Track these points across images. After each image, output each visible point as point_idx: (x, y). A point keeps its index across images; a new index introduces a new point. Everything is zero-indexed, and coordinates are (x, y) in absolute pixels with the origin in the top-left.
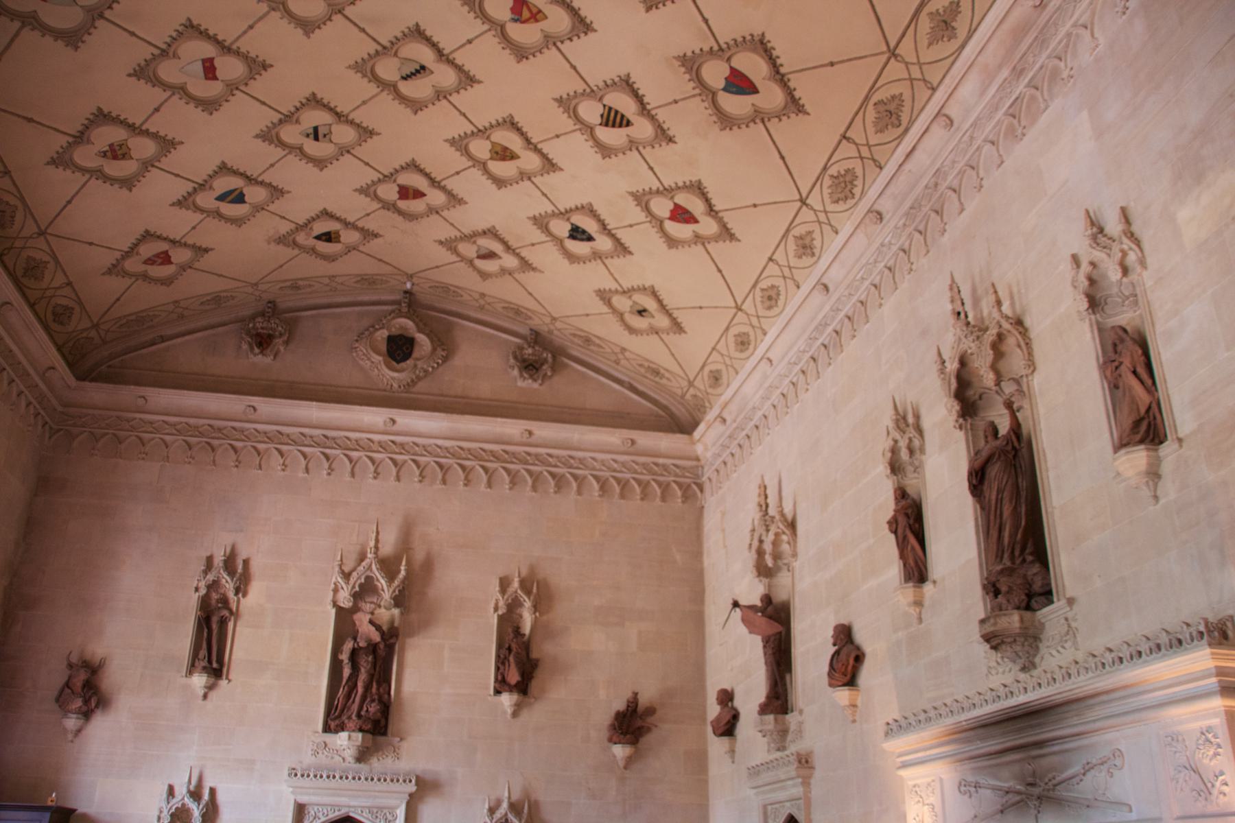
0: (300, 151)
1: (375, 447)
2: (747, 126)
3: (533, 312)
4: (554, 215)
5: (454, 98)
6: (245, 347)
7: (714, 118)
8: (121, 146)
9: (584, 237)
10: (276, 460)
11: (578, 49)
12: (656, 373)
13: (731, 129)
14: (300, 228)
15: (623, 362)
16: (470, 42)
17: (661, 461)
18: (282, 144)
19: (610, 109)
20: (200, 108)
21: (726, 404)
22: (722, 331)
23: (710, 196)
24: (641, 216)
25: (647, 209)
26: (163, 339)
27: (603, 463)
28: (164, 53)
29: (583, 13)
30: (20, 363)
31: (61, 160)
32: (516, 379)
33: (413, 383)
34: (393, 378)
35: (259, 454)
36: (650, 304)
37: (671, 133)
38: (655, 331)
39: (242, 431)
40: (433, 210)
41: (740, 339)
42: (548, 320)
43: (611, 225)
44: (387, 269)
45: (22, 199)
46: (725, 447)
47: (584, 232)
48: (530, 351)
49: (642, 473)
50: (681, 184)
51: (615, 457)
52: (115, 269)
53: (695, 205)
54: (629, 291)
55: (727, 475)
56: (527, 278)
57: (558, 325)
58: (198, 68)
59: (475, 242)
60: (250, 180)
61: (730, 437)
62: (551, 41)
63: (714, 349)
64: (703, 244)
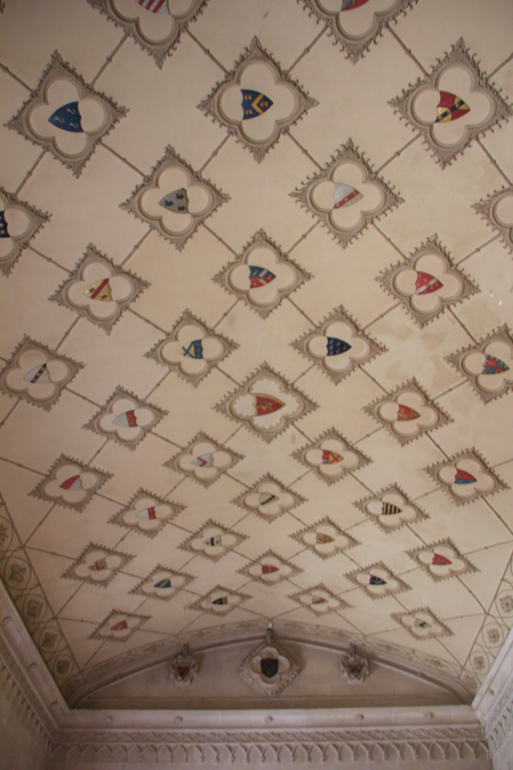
0: (203, 553)
1: (261, 738)
2: (473, 501)
3: (352, 633)
4: (359, 571)
5: (293, 511)
6: (172, 676)
7: (452, 500)
8: (101, 562)
9: (380, 582)
10: (197, 754)
11: (363, 473)
12: (438, 663)
13: (463, 504)
14: (203, 598)
15: (414, 659)
16: (299, 478)
17: (454, 727)
18: (193, 550)
19: (387, 505)
20: (146, 536)
21: (492, 681)
22: (478, 630)
23: (456, 546)
24: (414, 564)
25: (418, 560)
26: (121, 676)
27: (414, 733)
28: (127, 508)
29: (364, 453)
30: (38, 702)
31: (69, 574)
32: (346, 680)
33: (281, 690)
34: (268, 689)
35: (186, 750)
36: (428, 619)
37: (426, 513)
38: (434, 636)
39: (173, 735)
40: (284, 578)
41: (491, 634)
42: (361, 637)
43: (396, 572)
44: (255, 617)
45: (46, 599)
46: (497, 712)
47: (379, 579)
48: (352, 659)
49: (442, 738)
50: (437, 542)
51: (423, 727)
52: (95, 635)
53: (448, 553)
54: (412, 612)
55: (504, 733)
56: (346, 612)
57: (368, 639)
58: (146, 513)
59: (311, 594)
60: (174, 573)
61: (500, 703)
62: (347, 471)
63: (475, 643)
64: (457, 576)
